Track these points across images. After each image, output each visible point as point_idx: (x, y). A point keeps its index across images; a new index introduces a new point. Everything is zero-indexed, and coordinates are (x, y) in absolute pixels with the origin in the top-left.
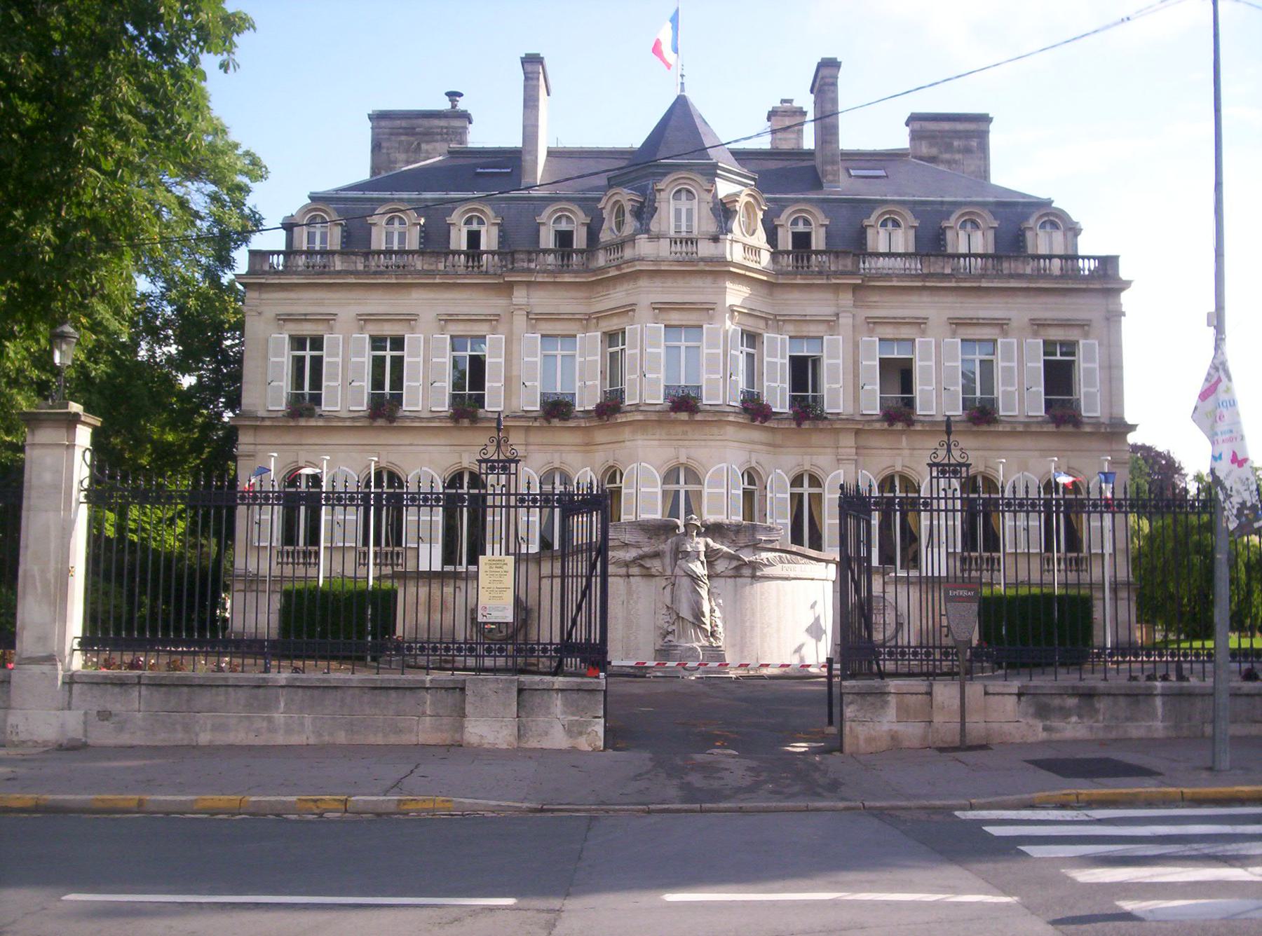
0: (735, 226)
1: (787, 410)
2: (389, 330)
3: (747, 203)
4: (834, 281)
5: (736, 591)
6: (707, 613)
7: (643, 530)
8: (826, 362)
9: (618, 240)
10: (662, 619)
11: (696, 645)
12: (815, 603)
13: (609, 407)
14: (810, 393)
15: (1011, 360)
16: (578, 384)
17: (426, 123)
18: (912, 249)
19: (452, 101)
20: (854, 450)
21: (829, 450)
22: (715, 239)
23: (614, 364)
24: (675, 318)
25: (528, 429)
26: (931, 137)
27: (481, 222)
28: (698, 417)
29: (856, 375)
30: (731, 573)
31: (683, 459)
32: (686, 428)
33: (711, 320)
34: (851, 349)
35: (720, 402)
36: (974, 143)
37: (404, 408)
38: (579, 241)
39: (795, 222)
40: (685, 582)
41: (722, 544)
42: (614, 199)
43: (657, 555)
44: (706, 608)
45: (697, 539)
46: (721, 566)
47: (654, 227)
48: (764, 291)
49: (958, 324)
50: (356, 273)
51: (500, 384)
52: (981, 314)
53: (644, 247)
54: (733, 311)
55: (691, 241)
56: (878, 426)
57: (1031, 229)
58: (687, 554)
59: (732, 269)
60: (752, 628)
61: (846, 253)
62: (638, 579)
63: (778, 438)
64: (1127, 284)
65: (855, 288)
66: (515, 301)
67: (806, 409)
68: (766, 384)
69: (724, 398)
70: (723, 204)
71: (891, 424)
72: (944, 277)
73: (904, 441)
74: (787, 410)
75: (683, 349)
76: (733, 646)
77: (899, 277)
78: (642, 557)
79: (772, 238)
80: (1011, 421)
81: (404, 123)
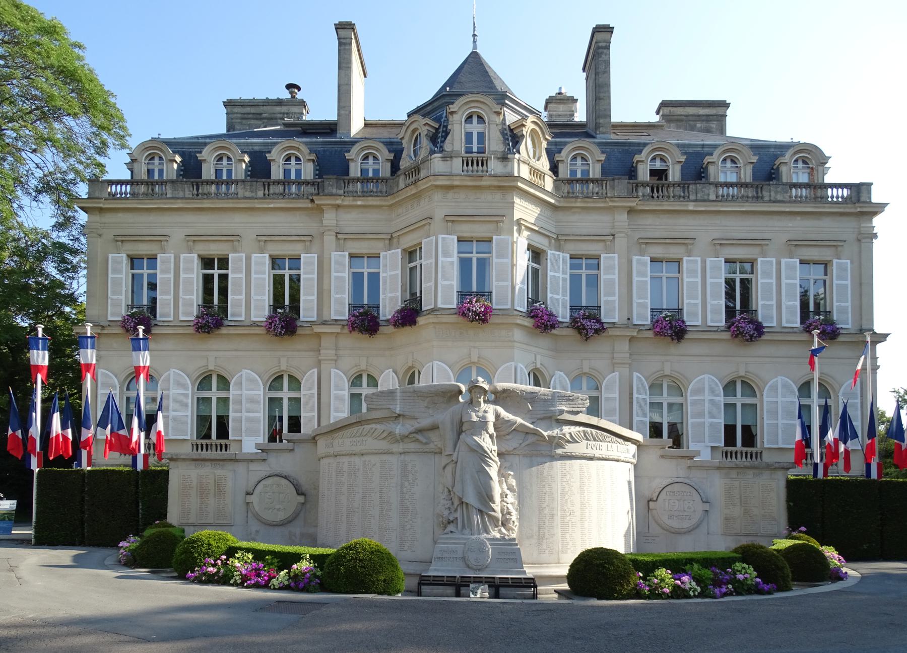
0: (522, 148)
3: (533, 130)
6: (497, 498)
19: (291, 93)
20: (628, 355)
23: (412, 276)
33: (498, 232)
42: (412, 128)
45: (483, 406)
47: (447, 146)
48: (548, 213)
53: (437, 164)
64: (881, 208)
68: (549, 295)
70: (511, 130)
75: (664, 279)
79: (554, 169)
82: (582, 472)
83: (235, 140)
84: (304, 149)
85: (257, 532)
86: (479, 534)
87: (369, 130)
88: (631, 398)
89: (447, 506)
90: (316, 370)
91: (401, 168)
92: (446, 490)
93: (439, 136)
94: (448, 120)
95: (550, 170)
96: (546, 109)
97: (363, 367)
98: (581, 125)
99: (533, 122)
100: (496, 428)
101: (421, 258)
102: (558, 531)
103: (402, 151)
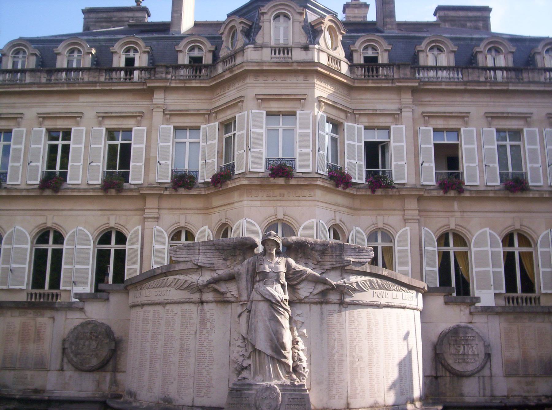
0: (321, 40)
1: (363, 181)
2: (61, 124)
4: (397, 84)
5: (322, 319)
7: (217, 250)
8: (393, 145)
9: (233, 53)
10: (238, 351)
11: (274, 383)
12: (408, 334)
13: (223, 178)
14: (380, 169)
15: (535, 144)
16: (201, 162)
17: (119, 14)
18: (452, 64)
21: (397, 212)
22: (306, 48)
24: (275, 106)
25: (160, 196)
26: (452, 21)
27: (136, 51)
28: (293, 182)
29: (417, 155)
30: (316, 298)
31: (280, 216)
32: (285, 192)
33: (303, 107)
34: (412, 135)
35: (310, 170)
36: (481, 24)
37: (68, 182)
38: (207, 59)
39: (366, 48)
40: (263, 307)
41: (306, 265)
43: (231, 278)
44: (287, 338)
45: (276, 259)
46: (305, 290)
47: (259, 39)
49: (491, 117)
50: (39, 84)
51: (141, 163)
52: (510, 110)
53: (251, 54)
54: (320, 101)
55: (287, 50)
56: (435, 193)
57: (539, 53)
58: (265, 275)
59: (319, 69)
60: (341, 361)
61: (405, 65)
62: (212, 306)
63: (357, 203)
65: (414, 91)
66: (155, 101)
67: (378, 181)
68: (347, 160)
69: (314, 168)
70: (312, 27)
71: (446, 192)
72: (478, 83)
73: (456, 206)
74: (363, 181)
75: (281, 131)
76: (320, 383)
77: (448, 83)
78: (217, 281)
79: (349, 56)
80: (538, 189)
81: (105, 15)
82: (369, 320)
83: (85, 38)
84: (141, 43)
85: (70, 376)
86: (270, 380)
87: (197, 29)
88: (421, 250)
89: (241, 353)
90: (140, 227)
91: (221, 56)
92: (241, 338)
93: (251, 32)
94: (260, 19)
95: (345, 57)
96: (344, 12)
97: (182, 224)
98: (372, 23)
99: (330, 20)
100: (287, 279)
101: (235, 130)
102: (348, 377)
103: (222, 43)
